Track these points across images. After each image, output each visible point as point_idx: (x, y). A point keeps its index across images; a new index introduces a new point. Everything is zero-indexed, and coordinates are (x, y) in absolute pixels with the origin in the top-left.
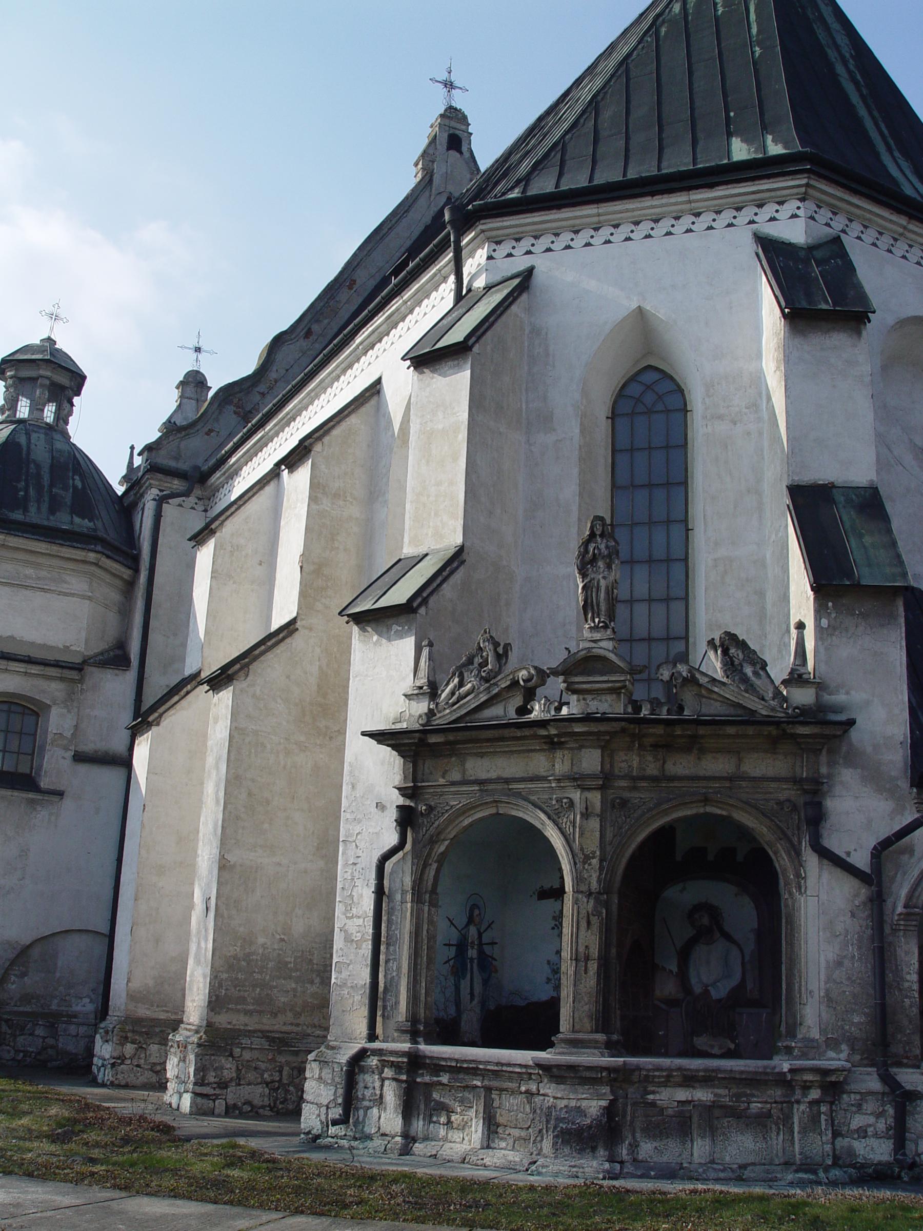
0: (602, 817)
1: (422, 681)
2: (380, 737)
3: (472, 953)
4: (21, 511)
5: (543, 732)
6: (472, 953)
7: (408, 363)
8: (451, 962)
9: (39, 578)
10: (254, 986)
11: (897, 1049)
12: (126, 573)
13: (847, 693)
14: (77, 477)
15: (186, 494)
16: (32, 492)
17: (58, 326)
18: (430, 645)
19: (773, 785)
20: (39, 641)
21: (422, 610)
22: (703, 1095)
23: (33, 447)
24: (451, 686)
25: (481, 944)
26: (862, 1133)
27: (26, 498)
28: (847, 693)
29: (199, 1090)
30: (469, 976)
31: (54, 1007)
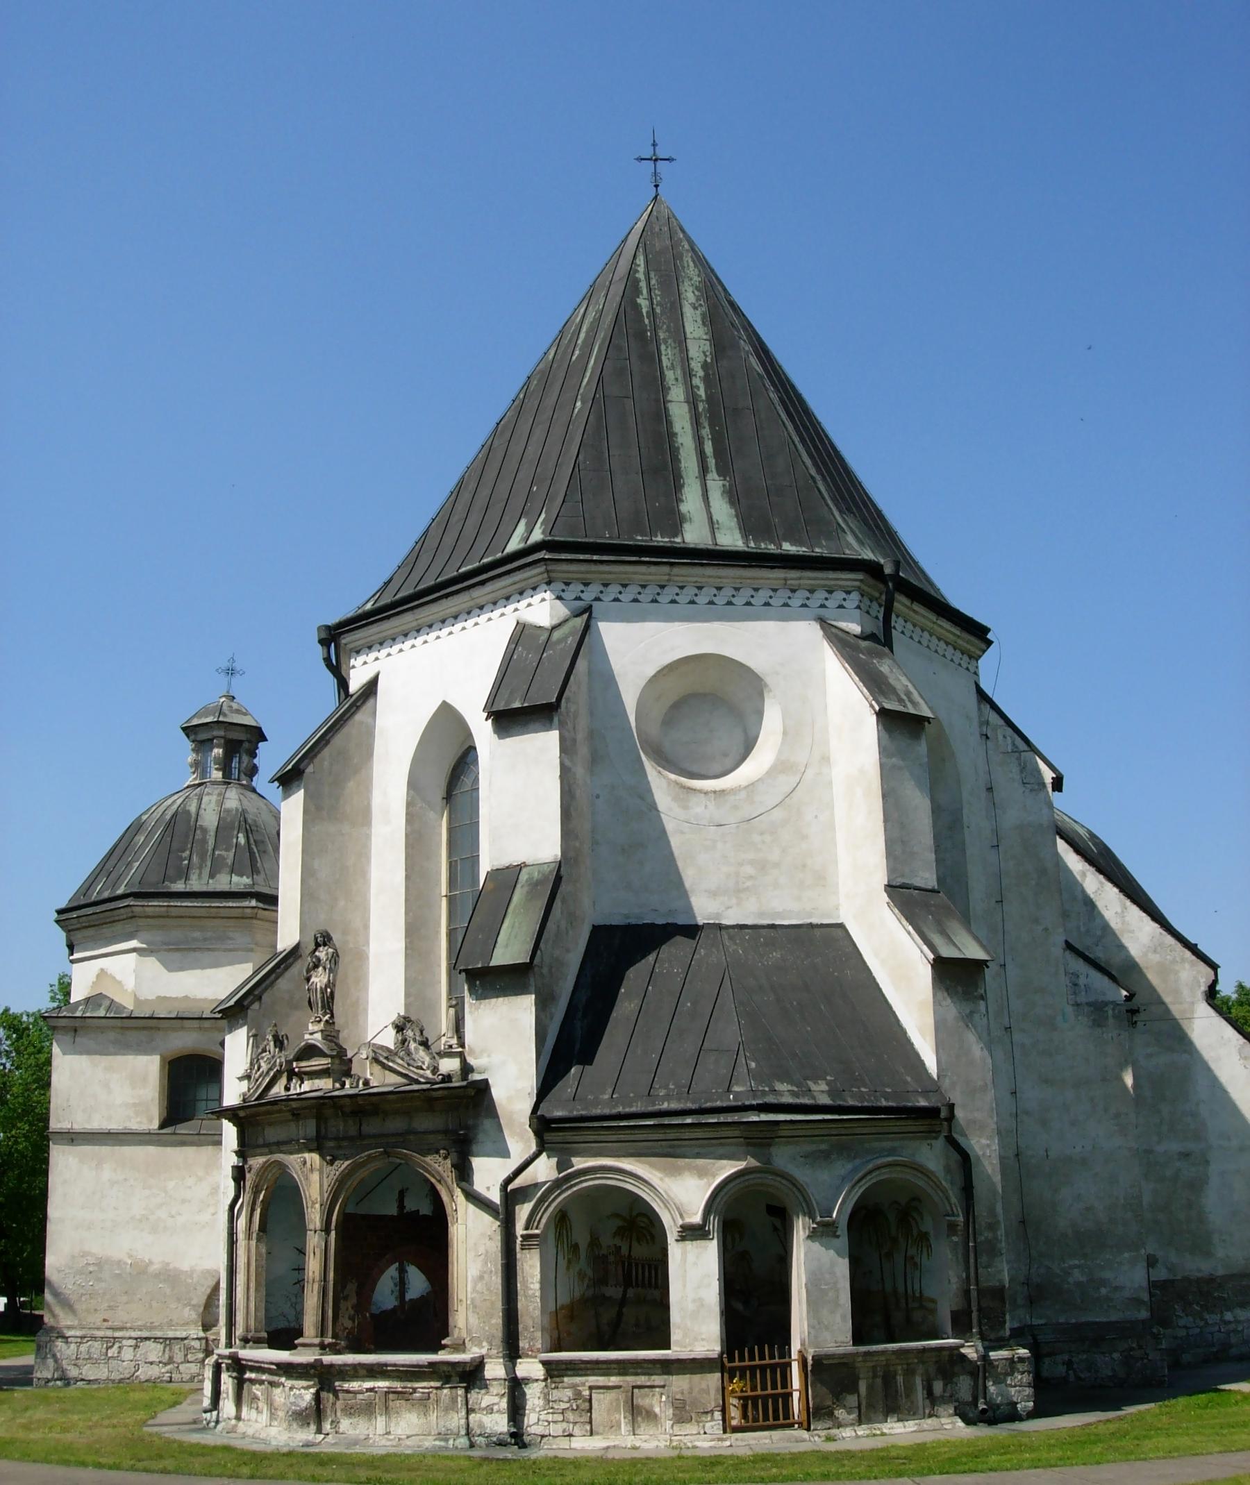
0: (321, 1173)
7: (276, 784)
9: (205, 939)
11: (523, 1344)
13: (489, 1056)
14: (241, 835)
16: (195, 858)
17: (236, 680)
21: (256, 1006)
22: (382, 1384)
23: (202, 812)
28: (489, 1056)
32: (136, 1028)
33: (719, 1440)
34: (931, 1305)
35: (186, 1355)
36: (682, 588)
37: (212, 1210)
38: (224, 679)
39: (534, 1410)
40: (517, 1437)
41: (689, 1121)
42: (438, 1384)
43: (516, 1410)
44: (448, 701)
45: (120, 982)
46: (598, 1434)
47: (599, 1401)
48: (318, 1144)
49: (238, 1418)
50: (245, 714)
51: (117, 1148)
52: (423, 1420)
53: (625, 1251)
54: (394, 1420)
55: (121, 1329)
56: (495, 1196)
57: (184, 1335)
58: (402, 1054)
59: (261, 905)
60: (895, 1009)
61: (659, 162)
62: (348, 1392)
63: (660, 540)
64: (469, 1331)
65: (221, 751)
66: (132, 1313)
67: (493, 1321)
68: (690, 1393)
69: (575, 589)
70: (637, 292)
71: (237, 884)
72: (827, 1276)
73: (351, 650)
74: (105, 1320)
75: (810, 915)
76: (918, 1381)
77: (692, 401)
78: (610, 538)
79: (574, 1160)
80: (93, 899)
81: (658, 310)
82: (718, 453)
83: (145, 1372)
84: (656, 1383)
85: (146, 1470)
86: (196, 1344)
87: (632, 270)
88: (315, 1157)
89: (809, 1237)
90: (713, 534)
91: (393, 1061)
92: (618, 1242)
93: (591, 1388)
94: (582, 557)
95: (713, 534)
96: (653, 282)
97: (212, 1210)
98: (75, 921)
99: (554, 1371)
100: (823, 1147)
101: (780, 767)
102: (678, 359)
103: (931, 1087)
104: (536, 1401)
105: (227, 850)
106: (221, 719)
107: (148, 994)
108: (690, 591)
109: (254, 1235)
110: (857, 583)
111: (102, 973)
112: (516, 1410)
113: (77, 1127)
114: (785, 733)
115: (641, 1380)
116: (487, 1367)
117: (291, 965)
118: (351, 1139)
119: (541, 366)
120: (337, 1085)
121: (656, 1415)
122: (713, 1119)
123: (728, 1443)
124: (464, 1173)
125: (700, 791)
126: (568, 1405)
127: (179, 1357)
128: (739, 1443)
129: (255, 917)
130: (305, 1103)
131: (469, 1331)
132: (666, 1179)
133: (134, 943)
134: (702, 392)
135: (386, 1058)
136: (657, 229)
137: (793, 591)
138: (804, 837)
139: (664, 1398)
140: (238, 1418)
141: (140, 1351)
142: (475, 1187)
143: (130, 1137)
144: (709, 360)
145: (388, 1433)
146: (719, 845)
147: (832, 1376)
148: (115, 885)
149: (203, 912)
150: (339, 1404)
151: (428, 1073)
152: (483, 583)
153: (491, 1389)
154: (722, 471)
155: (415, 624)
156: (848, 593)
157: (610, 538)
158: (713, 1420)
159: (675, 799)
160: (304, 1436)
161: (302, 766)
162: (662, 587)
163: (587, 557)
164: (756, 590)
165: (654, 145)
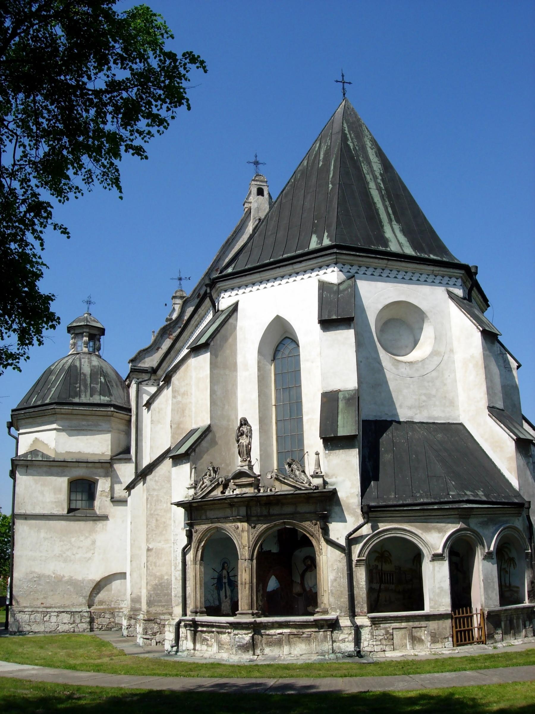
0: (248, 531)
1: (192, 482)
2: (179, 504)
3: (225, 580)
4: (78, 398)
5: (226, 502)
6: (225, 580)
8: (215, 585)
9: (88, 425)
10: (165, 595)
11: (357, 610)
12: (127, 417)
13: (336, 478)
14: (102, 378)
15: (149, 379)
16: (82, 388)
17: (91, 306)
18: (195, 468)
19: (308, 515)
20: (91, 452)
21: (193, 454)
22: (287, 631)
23: (82, 366)
24: (200, 485)
25: (229, 577)
26: (343, 641)
27: (80, 391)
28: (336, 478)
29: (145, 637)
30: (224, 589)
31: (113, 606)
32: (56, 466)
33: (452, 650)
34: (515, 589)
35: (81, 620)
36: (391, 271)
37: (92, 552)
38: (86, 306)
39: (366, 640)
40: (359, 654)
41: (436, 507)
42: (317, 630)
43: (357, 640)
44: (280, 315)
45: (46, 444)
46: (396, 650)
47: (397, 635)
48: (247, 519)
49: (194, 649)
50: (97, 322)
51: (47, 522)
52: (308, 647)
53: (380, 567)
54: (293, 648)
55: (50, 607)
56: (342, 542)
57: (80, 610)
58: (293, 476)
59: (115, 410)
60: (493, 460)
61: (342, 84)
62: (268, 635)
63: (381, 248)
64: (330, 605)
65: (87, 338)
66: (55, 600)
67: (342, 600)
68: (438, 629)
69: (347, 267)
70: (347, 139)
71: (104, 400)
72: (490, 576)
73: (222, 290)
74: (42, 604)
75: (449, 419)
76: (521, 622)
77: (379, 189)
78: (361, 245)
79: (380, 525)
80: (32, 405)
81: (357, 148)
82: (394, 213)
83: (62, 628)
84: (423, 626)
85: (332, 676)
86: (86, 614)
87: (343, 130)
88: (245, 525)
89: (483, 559)
90: (401, 248)
91: (287, 480)
92: (376, 563)
93: (393, 629)
94: (352, 253)
95: (401, 248)
96: (352, 135)
97: (92, 552)
98: (22, 415)
99: (375, 622)
100: (486, 519)
101: (434, 353)
102: (370, 170)
103: (517, 494)
104: (367, 636)
105: (97, 384)
106: (88, 324)
107: (62, 450)
108: (394, 272)
109: (198, 562)
110: (461, 275)
111: (36, 439)
112: (357, 640)
113: (28, 512)
114: (435, 338)
115: (417, 624)
116: (340, 621)
117: (208, 434)
118: (265, 516)
119: (300, 168)
120: (256, 491)
121: (423, 640)
122: (447, 507)
123: (457, 651)
124: (325, 531)
125: (402, 362)
126: (383, 637)
127: (78, 621)
128: (462, 651)
129: (112, 416)
130: (243, 499)
131: (330, 605)
132: (424, 534)
133: (54, 426)
134: (382, 186)
135: (284, 478)
136: (349, 113)
137: (436, 276)
138: (445, 385)
139: (426, 632)
140: (194, 649)
141: (59, 618)
142: (330, 537)
143: (54, 517)
144: (382, 172)
145: (290, 654)
146: (412, 386)
147: (493, 619)
148: (44, 398)
149: (88, 413)
150: (264, 641)
151: (307, 485)
152: (300, 262)
153: (344, 631)
154: (398, 221)
155: (260, 279)
156: (457, 279)
157: (361, 245)
158: (448, 641)
159: (393, 365)
160: (246, 657)
161: (209, 342)
162: (383, 270)
163: (354, 253)
164: (421, 274)
165: (343, 76)
